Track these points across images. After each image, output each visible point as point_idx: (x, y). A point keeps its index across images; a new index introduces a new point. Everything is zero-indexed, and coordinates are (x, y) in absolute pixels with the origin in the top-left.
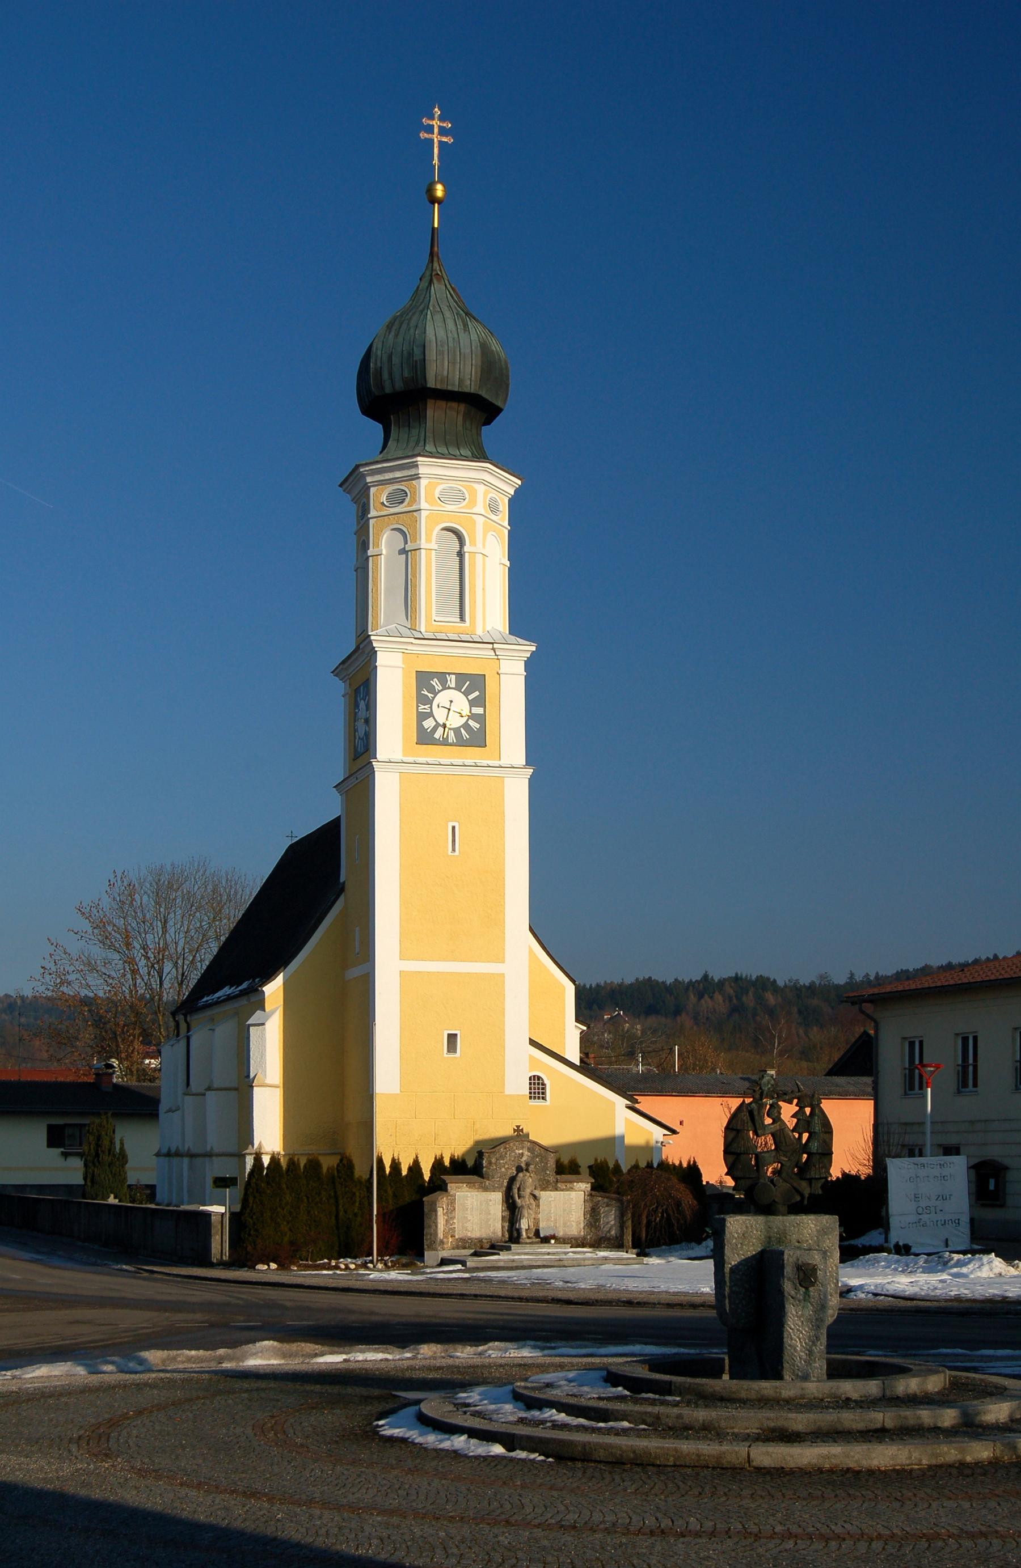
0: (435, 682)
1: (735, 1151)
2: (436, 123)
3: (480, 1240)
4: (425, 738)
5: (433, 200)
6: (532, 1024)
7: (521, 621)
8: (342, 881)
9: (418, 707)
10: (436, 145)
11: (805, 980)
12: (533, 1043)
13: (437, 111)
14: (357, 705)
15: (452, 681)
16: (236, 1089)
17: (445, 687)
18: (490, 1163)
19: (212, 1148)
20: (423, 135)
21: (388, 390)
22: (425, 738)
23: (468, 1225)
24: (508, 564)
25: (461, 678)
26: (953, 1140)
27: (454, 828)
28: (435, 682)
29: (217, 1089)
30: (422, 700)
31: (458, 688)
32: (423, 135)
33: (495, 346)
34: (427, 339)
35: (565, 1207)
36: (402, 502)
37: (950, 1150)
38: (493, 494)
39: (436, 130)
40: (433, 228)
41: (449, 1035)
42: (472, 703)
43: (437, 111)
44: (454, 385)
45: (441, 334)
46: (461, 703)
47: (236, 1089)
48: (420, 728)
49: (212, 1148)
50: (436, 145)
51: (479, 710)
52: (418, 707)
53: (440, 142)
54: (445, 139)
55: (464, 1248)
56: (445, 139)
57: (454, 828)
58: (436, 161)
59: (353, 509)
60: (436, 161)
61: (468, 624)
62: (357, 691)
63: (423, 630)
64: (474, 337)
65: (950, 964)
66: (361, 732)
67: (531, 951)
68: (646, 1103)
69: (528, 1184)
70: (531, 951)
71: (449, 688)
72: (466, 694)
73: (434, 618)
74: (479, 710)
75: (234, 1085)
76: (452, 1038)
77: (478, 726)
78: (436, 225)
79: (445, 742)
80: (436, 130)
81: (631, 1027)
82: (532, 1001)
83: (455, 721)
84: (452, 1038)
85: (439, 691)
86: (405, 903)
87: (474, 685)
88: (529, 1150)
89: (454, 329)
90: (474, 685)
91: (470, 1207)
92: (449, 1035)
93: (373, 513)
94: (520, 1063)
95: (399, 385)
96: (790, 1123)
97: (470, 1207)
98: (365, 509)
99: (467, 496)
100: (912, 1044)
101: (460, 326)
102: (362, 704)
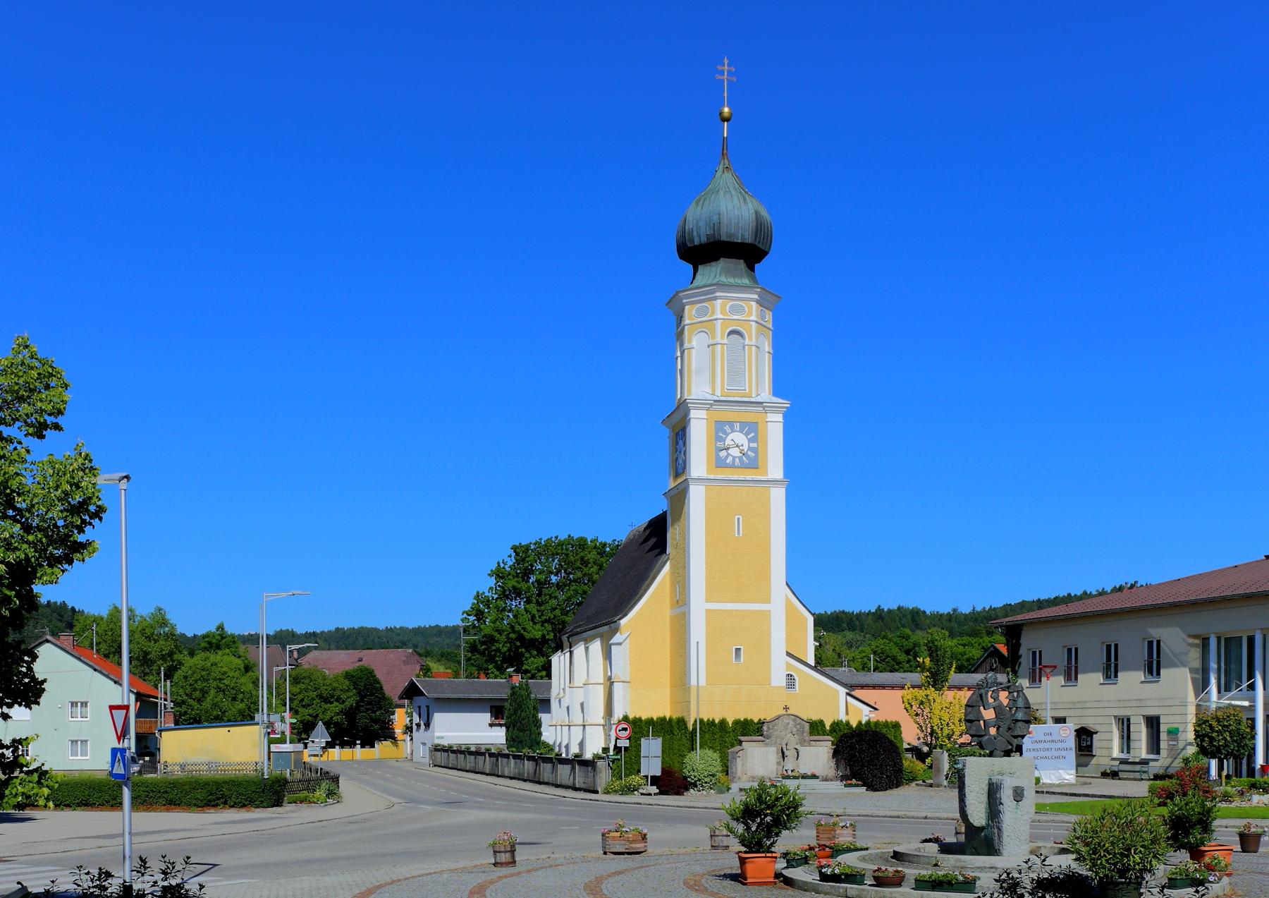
0: (727, 428)
1: (971, 721)
4: (720, 464)
6: (788, 640)
7: (778, 389)
11: (965, 609)
12: (789, 654)
13: (726, 62)
14: (677, 443)
15: (737, 426)
20: (719, 77)
21: (697, 243)
22: (720, 464)
25: (743, 425)
26: (1061, 714)
28: (727, 428)
30: (718, 439)
31: (741, 431)
32: (719, 77)
33: (764, 212)
35: (819, 756)
37: (1060, 720)
42: (750, 441)
46: (740, 438)
48: (718, 457)
51: (754, 445)
59: (674, 319)
62: (677, 434)
64: (750, 206)
65: (1069, 595)
67: (787, 597)
68: (857, 693)
70: (787, 597)
72: (746, 435)
74: (754, 445)
76: (738, 650)
79: (732, 466)
81: (851, 640)
82: (786, 628)
84: (738, 650)
87: (752, 429)
90: (752, 429)
93: (687, 321)
94: (779, 666)
95: (704, 240)
96: (1005, 702)
98: (680, 318)
100: (1034, 653)
102: (681, 442)
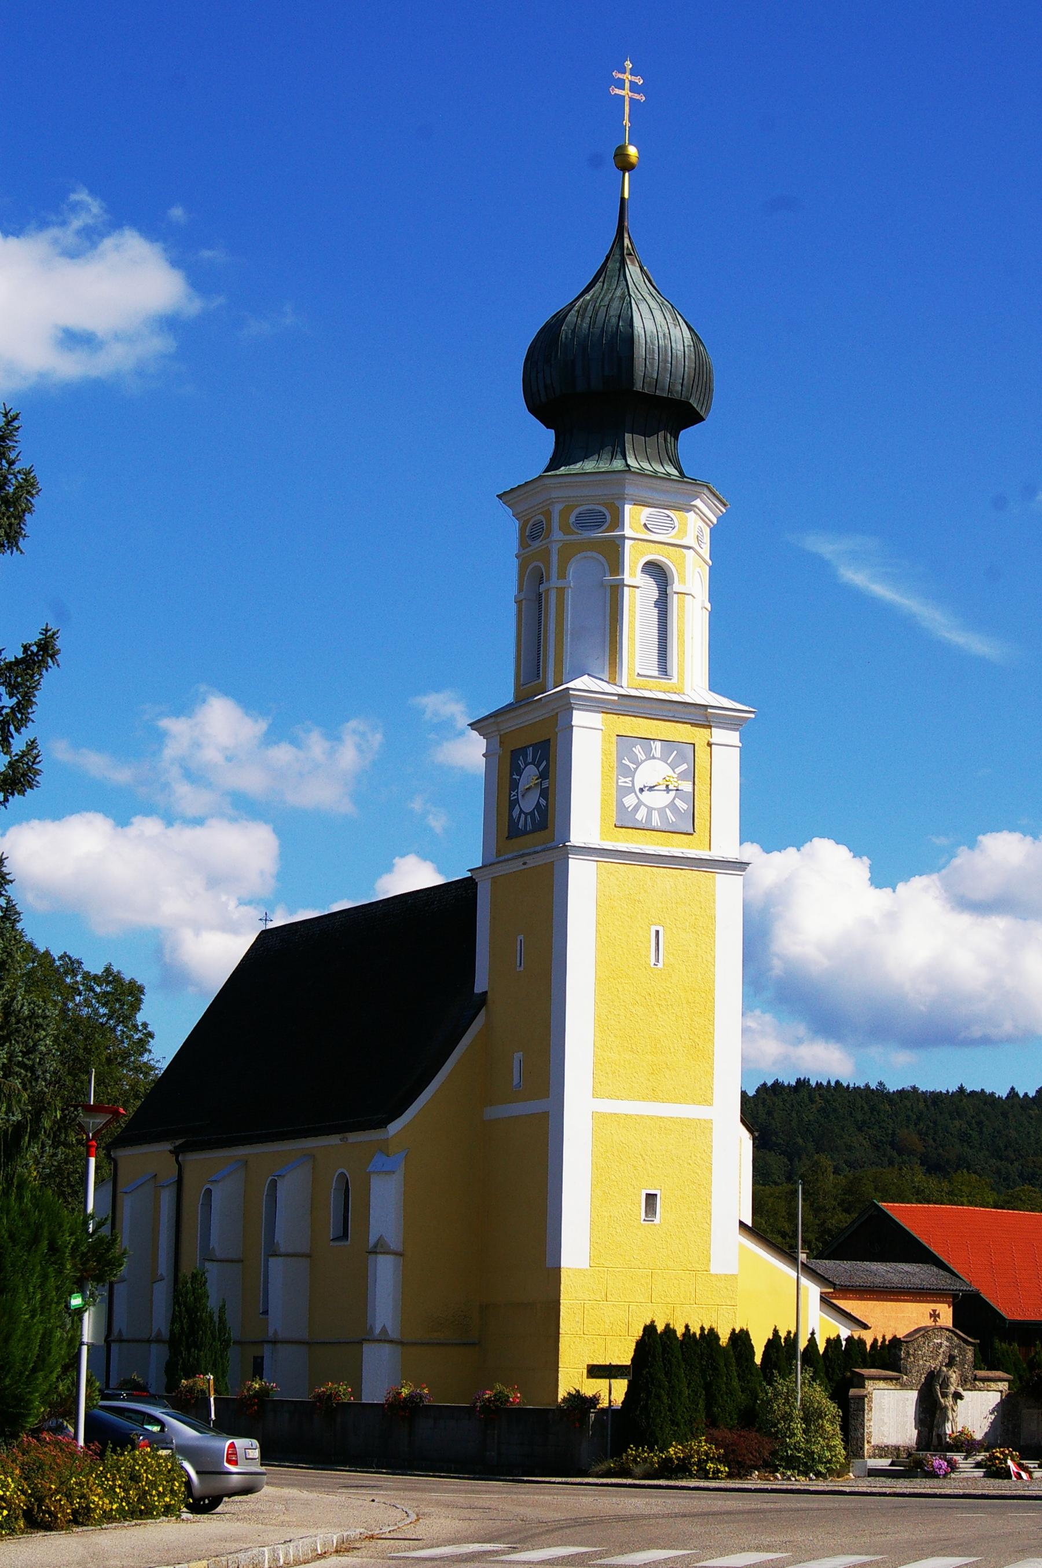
0: (638, 750)
2: (627, 77)
3: (897, 1448)
5: (624, 164)
8: (478, 989)
9: (618, 779)
10: (627, 103)
13: (628, 65)
16: (308, 1256)
17: (650, 757)
18: (908, 1354)
19: (276, 1332)
23: (885, 1428)
24: (708, 606)
27: (657, 932)
28: (638, 750)
29: (287, 1255)
34: (636, 332)
36: (600, 526)
38: (702, 524)
39: (627, 85)
40: (623, 199)
41: (648, 1195)
43: (628, 65)
44: (663, 390)
45: (650, 326)
47: (308, 1256)
48: (621, 807)
49: (276, 1332)
50: (627, 103)
52: (618, 779)
53: (631, 98)
54: (637, 97)
55: (881, 1457)
56: (637, 97)
57: (657, 932)
58: (626, 122)
60: (626, 122)
61: (675, 680)
63: (624, 684)
66: (528, 803)
69: (952, 1380)
71: (654, 758)
73: (638, 670)
75: (400, 1249)
76: (651, 1198)
77: (685, 807)
78: (626, 196)
80: (627, 85)
83: (659, 800)
84: (651, 1198)
85: (643, 761)
86: (601, 1025)
88: (948, 1339)
89: (664, 322)
91: (887, 1406)
92: (648, 1195)
97: (887, 1406)
99: (676, 524)
101: (670, 320)
